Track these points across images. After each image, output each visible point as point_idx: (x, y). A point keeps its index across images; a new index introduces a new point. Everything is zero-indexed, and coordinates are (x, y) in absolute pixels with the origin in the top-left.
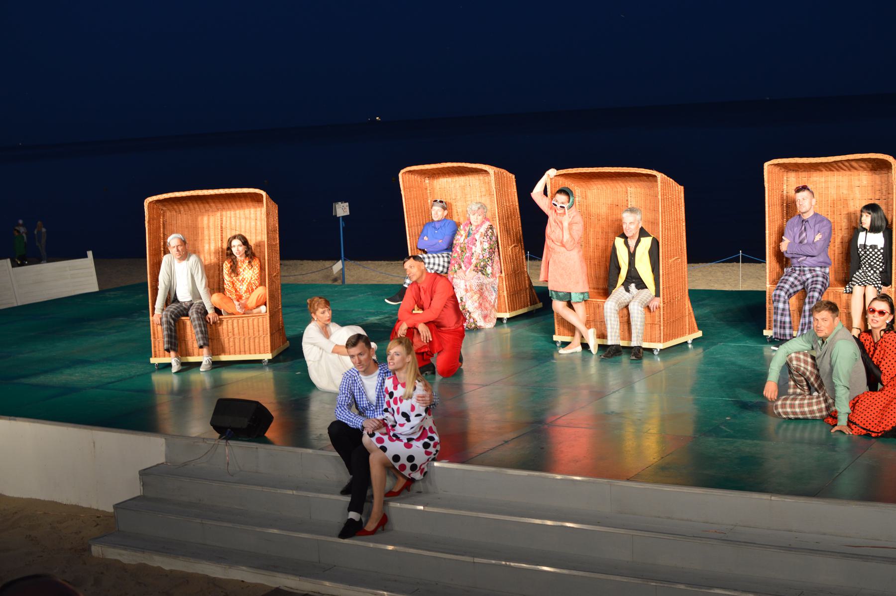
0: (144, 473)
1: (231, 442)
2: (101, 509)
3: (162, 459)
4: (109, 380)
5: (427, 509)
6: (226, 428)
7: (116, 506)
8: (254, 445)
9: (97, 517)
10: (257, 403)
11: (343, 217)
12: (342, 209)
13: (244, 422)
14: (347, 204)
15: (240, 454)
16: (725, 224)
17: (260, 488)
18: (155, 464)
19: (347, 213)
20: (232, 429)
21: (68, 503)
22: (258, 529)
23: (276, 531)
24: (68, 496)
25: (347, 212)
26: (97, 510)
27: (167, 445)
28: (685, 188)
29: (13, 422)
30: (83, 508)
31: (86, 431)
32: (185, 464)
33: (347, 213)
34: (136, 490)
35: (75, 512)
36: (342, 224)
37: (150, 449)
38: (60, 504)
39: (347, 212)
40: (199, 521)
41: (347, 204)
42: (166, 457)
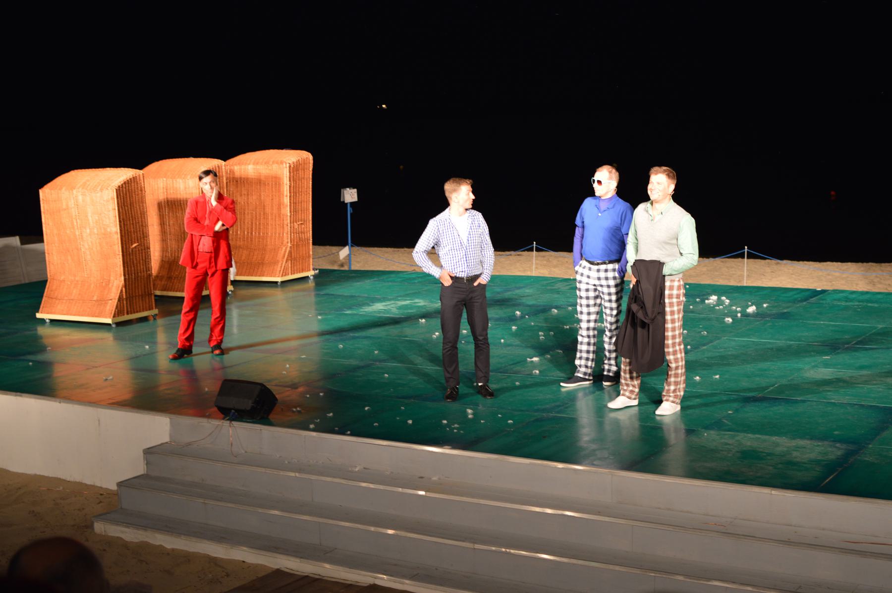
0: (149, 452)
2: (104, 486)
3: (166, 439)
6: (230, 410)
7: (120, 484)
8: (258, 427)
9: (101, 494)
10: (262, 385)
11: (352, 203)
12: (350, 195)
13: (248, 404)
19: (355, 199)
20: (236, 410)
21: (72, 479)
25: (355, 198)
28: (42, 186)
30: (86, 485)
32: (189, 444)
33: (355, 199)
34: (139, 468)
35: (79, 489)
39: (355, 198)
42: (171, 436)
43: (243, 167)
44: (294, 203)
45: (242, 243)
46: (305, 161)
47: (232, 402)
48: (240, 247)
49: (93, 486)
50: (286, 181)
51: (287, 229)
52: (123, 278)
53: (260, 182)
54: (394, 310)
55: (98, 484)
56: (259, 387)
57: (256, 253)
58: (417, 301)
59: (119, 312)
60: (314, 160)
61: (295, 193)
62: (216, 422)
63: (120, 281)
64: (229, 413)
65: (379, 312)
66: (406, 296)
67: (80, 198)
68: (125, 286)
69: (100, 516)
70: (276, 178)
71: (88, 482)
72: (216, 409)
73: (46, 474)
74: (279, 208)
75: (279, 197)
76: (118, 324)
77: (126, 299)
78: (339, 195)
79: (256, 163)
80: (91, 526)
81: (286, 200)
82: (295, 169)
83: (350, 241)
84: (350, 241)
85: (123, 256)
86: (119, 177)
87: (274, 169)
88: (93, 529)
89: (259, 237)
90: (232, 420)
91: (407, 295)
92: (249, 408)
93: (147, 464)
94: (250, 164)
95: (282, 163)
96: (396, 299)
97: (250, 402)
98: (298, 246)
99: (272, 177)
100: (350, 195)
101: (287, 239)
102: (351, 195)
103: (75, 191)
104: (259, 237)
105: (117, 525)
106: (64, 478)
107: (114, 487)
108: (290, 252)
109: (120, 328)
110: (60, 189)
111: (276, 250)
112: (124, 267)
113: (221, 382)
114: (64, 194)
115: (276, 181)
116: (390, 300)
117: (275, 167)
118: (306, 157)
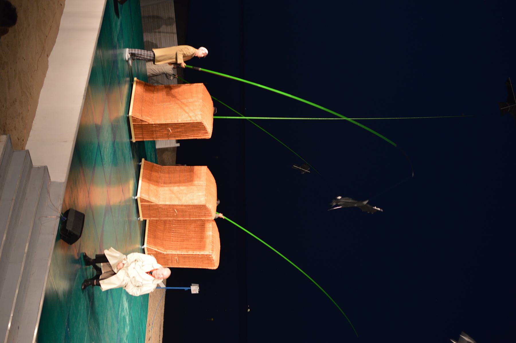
0: (45, 169)
1: (59, 220)
2: (28, 142)
3: (52, 179)
4: (102, 153)
5: (8, 332)
6: (67, 217)
7: (28, 152)
8: (56, 233)
9: (23, 141)
10: (80, 236)
11: (190, 290)
12: (195, 289)
13: (69, 227)
14: (198, 292)
15: (51, 224)
16: (190, 153)
17: (30, 234)
18: (50, 175)
19: (193, 292)
20: (66, 221)
21: (33, 124)
22: (6, 232)
23: (4, 238)
24: (37, 124)
25: (193, 292)
26: (27, 140)
27: (60, 183)
28: (205, 84)
29: (82, 97)
30: (29, 132)
31: (80, 108)
32: (48, 192)
33: (193, 292)
34: (36, 164)
35: (28, 128)
36: (186, 289)
37: (59, 173)
38: (33, 119)
39: (193, 292)
40: (14, 198)
41: (198, 292)
42: (54, 182)
43: (211, 229)
44: (189, 257)
45: (168, 227)
46: (213, 265)
47: (71, 218)
48: (165, 225)
49: (29, 136)
50: (202, 253)
51: (174, 252)
52: (153, 123)
53: (202, 237)
54: (123, 314)
55: (29, 139)
56: (79, 235)
57: (161, 234)
58: (128, 327)
59: (135, 120)
60: (214, 270)
61: (195, 258)
62: (60, 209)
63: (151, 122)
64: (65, 215)
65: (123, 305)
66: (131, 321)
67: (198, 104)
68: (149, 124)
69: (10, 138)
70: (204, 247)
71: (31, 133)
72: (68, 209)
73: (38, 110)
74: (186, 248)
75: (193, 249)
76: (128, 118)
77: (142, 125)
78: (195, 283)
79: (213, 236)
80: (4, 133)
81: (190, 253)
82: (208, 258)
83: (168, 288)
84: (168, 288)
85: (165, 124)
86: (208, 125)
87: (209, 246)
88: (2, 135)
89: (170, 236)
90: (61, 218)
91: (132, 321)
92: (67, 228)
93: (39, 168)
94: (212, 234)
95: (212, 250)
96: (130, 315)
97: (71, 229)
98: (164, 258)
99: (205, 245)
100: (195, 289)
101: (170, 252)
102: (195, 290)
103: (201, 101)
104: (170, 236)
105: (4, 149)
106: (35, 119)
107: (27, 148)
108: (161, 253)
109: (126, 119)
110: (203, 94)
111: (162, 246)
112: (159, 124)
113: (83, 212)
114: (201, 95)
115: (202, 247)
116: (130, 312)
117: (211, 247)
118: (215, 266)
